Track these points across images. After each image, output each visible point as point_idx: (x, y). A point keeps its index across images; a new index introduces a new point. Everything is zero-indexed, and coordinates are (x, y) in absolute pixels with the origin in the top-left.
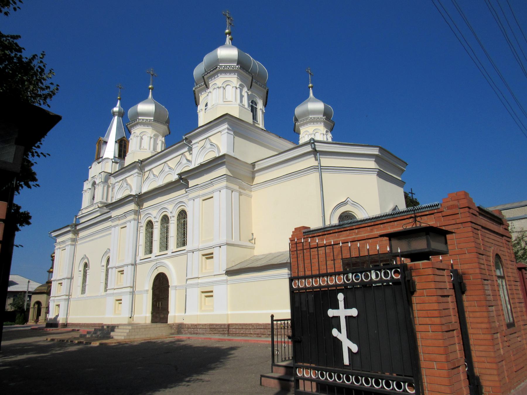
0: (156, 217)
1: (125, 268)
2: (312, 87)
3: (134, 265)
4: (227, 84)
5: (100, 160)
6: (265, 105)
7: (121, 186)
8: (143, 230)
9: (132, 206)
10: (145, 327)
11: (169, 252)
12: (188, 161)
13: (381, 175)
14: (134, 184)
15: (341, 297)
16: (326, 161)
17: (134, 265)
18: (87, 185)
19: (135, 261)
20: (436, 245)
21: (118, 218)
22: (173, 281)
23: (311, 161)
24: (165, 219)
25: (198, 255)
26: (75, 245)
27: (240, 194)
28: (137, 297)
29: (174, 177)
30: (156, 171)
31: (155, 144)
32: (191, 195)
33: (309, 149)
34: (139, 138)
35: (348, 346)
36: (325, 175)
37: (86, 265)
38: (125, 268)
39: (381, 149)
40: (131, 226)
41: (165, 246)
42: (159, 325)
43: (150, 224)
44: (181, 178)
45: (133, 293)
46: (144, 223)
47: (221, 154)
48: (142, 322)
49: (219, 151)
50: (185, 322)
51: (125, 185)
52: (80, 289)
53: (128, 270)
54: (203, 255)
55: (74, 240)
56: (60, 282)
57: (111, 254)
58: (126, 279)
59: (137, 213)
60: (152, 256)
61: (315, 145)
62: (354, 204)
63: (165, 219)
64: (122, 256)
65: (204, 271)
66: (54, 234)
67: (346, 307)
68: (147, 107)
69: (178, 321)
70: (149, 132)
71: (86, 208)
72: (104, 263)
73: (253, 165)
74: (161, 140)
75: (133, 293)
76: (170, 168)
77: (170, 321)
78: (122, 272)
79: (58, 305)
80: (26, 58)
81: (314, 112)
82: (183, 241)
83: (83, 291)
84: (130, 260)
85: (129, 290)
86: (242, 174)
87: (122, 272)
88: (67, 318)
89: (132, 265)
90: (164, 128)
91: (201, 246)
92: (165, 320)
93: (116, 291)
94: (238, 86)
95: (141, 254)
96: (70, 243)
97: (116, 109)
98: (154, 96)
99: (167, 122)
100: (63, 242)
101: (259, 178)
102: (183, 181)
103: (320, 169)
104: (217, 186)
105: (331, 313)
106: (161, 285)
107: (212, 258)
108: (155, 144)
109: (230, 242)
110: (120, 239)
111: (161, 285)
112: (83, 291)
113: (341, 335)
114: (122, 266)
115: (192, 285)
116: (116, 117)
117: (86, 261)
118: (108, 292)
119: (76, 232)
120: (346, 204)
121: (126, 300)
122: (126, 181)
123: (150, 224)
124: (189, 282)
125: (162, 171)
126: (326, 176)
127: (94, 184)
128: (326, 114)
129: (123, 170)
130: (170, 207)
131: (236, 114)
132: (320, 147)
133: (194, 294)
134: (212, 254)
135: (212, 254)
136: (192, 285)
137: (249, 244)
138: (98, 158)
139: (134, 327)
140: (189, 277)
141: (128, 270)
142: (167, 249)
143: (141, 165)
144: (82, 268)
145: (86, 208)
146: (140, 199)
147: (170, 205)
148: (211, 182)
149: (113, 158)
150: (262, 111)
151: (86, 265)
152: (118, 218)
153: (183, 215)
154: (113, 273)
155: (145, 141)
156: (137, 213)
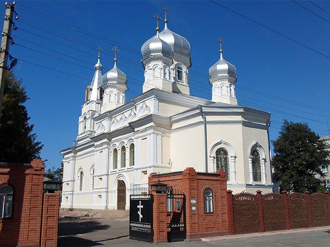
0: (118, 146)
2: (222, 52)
6: (189, 67)
7: (99, 127)
9: (106, 140)
12: (135, 114)
13: (245, 124)
14: (107, 126)
15: (140, 202)
16: (209, 118)
17: (108, 175)
18: (81, 119)
19: (108, 173)
21: (98, 146)
23: (200, 119)
24: (124, 148)
26: (75, 160)
27: (163, 137)
31: (119, 99)
33: (198, 111)
34: (109, 95)
35: (141, 216)
36: (208, 126)
37: (82, 173)
39: (244, 109)
40: (105, 151)
41: (124, 165)
42: (122, 211)
43: (115, 150)
44: (130, 126)
45: (107, 192)
46: (112, 151)
49: (150, 111)
52: (79, 187)
54: (142, 172)
55: (74, 157)
56: (67, 183)
58: (103, 184)
61: (202, 109)
63: (124, 148)
64: (100, 170)
65: (143, 181)
66: (62, 153)
67: (141, 205)
68: (112, 74)
70: (115, 91)
71: (81, 134)
72: (92, 172)
73: (170, 117)
74: (122, 95)
77: (126, 209)
78: (101, 179)
79: (67, 198)
81: (222, 71)
83: (81, 189)
84: (105, 172)
86: (163, 125)
87: (101, 179)
88: (72, 205)
89: (106, 175)
90: (124, 87)
93: (98, 190)
94: (162, 67)
95: (111, 169)
96: (72, 158)
97: (97, 65)
99: (126, 83)
100: (68, 158)
101: (175, 126)
102: (131, 127)
103: (205, 123)
104: (148, 132)
105: (138, 207)
108: (119, 99)
109: (156, 164)
110: (98, 159)
112: (81, 189)
113: (139, 213)
114: (101, 176)
116: (98, 71)
117: (81, 170)
119: (76, 152)
120: (221, 143)
121: (104, 195)
123: (115, 150)
125: (121, 119)
127: (85, 118)
128: (230, 72)
130: (126, 141)
131: (160, 87)
132: (204, 110)
134: (146, 171)
135: (146, 171)
137: (168, 166)
138: (87, 100)
139: (106, 210)
141: (104, 178)
143: (110, 114)
144: (79, 175)
145: (81, 134)
146: (110, 136)
147: (125, 139)
148: (146, 130)
149: (96, 100)
150: (186, 73)
151: (82, 173)
152: (98, 146)
153: (132, 146)
154: (96, 179)
155: (114, 98)
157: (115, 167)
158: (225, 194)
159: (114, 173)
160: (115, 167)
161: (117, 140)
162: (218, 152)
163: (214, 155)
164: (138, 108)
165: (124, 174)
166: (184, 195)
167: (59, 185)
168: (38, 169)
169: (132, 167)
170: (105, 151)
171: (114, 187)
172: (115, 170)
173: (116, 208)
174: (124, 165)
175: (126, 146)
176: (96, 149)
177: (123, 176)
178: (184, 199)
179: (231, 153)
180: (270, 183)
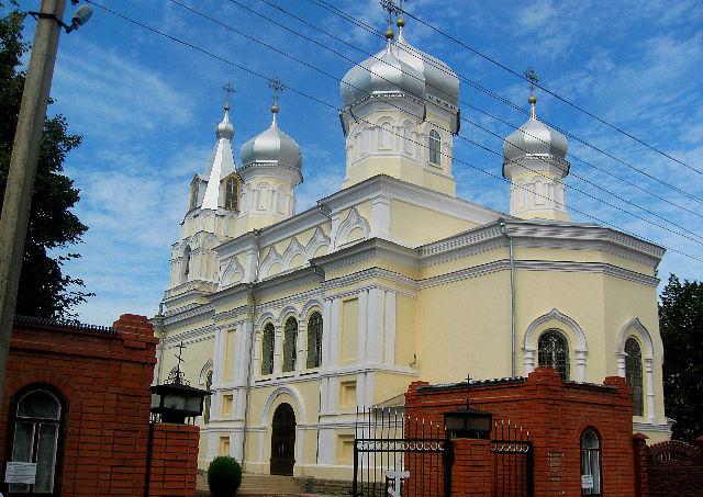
0: (277, 316)
1: (234, 393)
3: (249, 388)
4: (386, 121)
5: (197, 212)
8: (259, 338)
9: (244, 302)
10: (262, 479)
11: (296, 374)
16: (524, 254)
20: (194, 406)
21: (225, 315)
22: (302, 418)
23: (500, 254)
24: (292, 324)
25: (335, 383)
28: (251, 436)
29: (305, 264)
30: (280, 249)
32: (329, 293)
38: (234, 393)
40: (243, 332)
41: (290, 364)
43: (270, 329)
46: (261, 329)
47: (371, 236)
48: (257, 472)
50: (316, 477)
51: (235, 266)
53: (239, 396)
57: (214, 369)
59: (253, 310)
60: (273, 377)
62: (564, 319)
63: (292, 324)
69: (308, 474)
70: (272, 184)
73: (419, 250)
75: (245, 430)
76: (300, 246)
77: (297, 473)
80: (96, 181)
82: (315, 360)
84: (240, 382)
85: (239, 425)
87: (230, 398)
91: (339, 370)
92: (290, 472)
93: (222, 425)
95: (257, 375)
98: (279, 126)
102: (317, 268)
104: (240, 318)
106: (284, 422)
107: (355, 387)
111: (284, 422)
114: (355, 373)
115: (327, 427)
118: (210, 426)
122: (236, 259)
123: (270, 329)
124: (323, 421)
126: (524, 277)
129: (341, 194)
133: (329, 439)
134: (355, 382)
135: (355, 382)
136: (327, 427)
140: (323, 413)
141: (239, 396)
142: (293, 370)
143: (259, 238)
146: (256, 290)
148: (356, 278)
152: (225, 315)
153: (316, 323)
156: (253, 310)
157: (268, 367)
158: (626, 444)
159: (262, 385)
160: (268, 367)
161: (274, 304)
162: (545, 339)
163: (533, 345)
164: (336, 224)
165: (290, 386)
166: (530, 444)
167: (487, 421)
168: (136, 345)
169: (315, 370)
170: (243, 332)
171: (264, 421)
172: (266, 378)
173: (267, 470)
174: (290, 364)
175: (275, 324)
176: (217, 325)
177: (289, 393)
178: (530, 458)
179: (575, 344)
180: (664, 421)
